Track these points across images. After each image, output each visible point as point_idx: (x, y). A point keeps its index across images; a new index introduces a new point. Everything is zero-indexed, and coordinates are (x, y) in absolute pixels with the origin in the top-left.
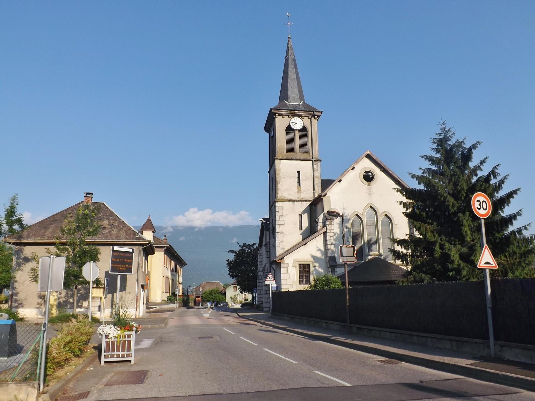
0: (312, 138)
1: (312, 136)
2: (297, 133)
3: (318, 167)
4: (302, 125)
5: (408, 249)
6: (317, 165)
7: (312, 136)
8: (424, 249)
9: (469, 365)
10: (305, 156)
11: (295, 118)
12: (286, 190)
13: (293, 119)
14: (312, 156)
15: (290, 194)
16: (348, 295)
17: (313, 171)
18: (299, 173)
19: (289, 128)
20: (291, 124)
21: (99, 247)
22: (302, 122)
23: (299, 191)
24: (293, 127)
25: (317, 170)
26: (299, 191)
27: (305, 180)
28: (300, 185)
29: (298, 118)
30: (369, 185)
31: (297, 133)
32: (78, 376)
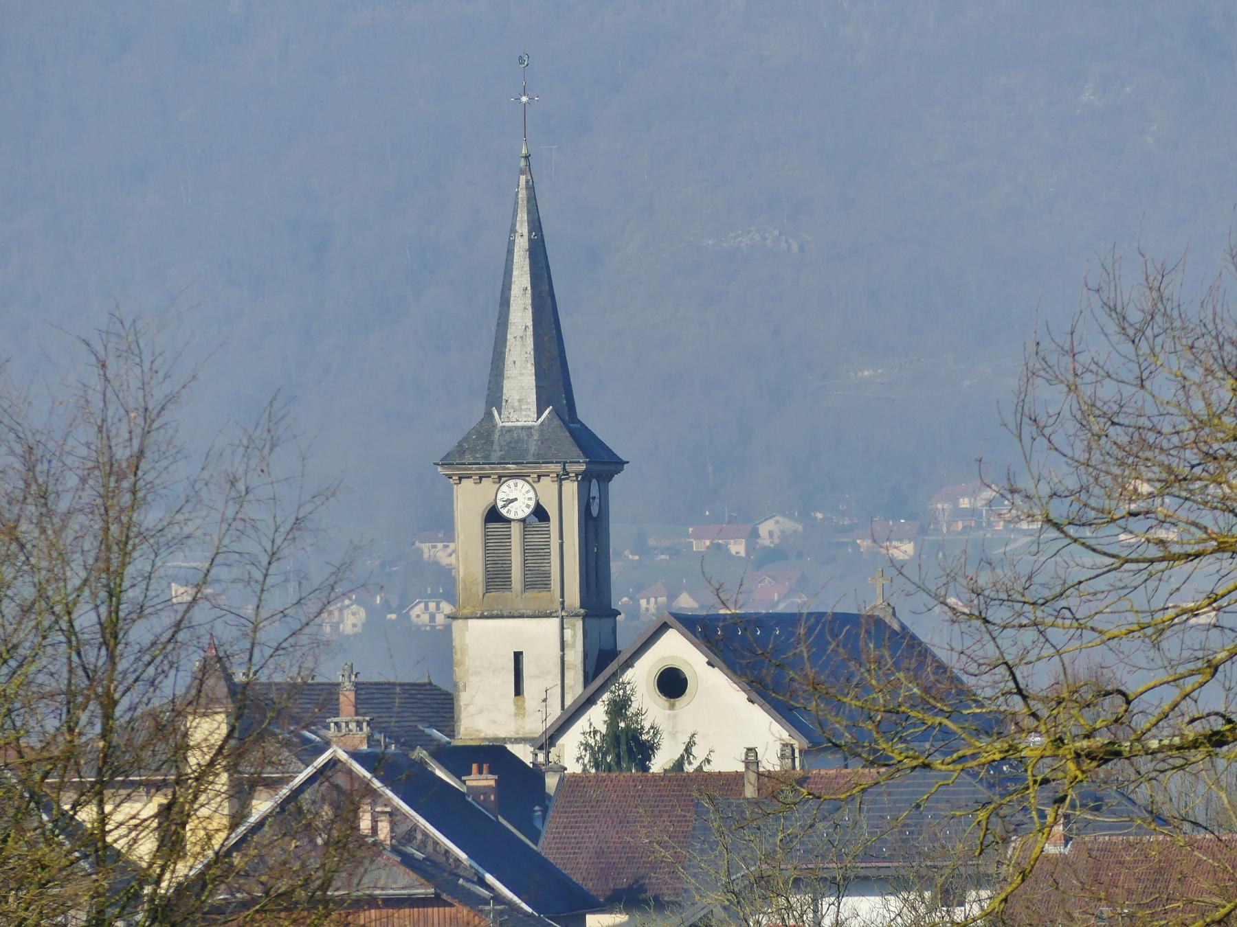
0: (561, 546)
1: (561, 537)
2: (516, 529)
3: (574, 636)
4: (532, 504)
5: (422, 764)
6: (573, 627)
7: (561, 537)
8: (535, 776)
9: (403, 888)
10: (537, 598)
11: (511, 482)
12: (481, 712)
13: (504, 488)
14: (563, 603)
15: (494, 722)
16: (530, 910)
17: (563, 649)
18: (518, 656)
19: (493, 515)
20: (500, 504)
21: (1162, 554)
22: (532, 494)
23: (520, 711)
24: (504, 512)
25: (573, 645)
26: (520, 711)
27: (537, 677)
28: (518, 691)
29: (520, 483)
30: (672, 707)
31: (516, 529)
32: (1025, 848)
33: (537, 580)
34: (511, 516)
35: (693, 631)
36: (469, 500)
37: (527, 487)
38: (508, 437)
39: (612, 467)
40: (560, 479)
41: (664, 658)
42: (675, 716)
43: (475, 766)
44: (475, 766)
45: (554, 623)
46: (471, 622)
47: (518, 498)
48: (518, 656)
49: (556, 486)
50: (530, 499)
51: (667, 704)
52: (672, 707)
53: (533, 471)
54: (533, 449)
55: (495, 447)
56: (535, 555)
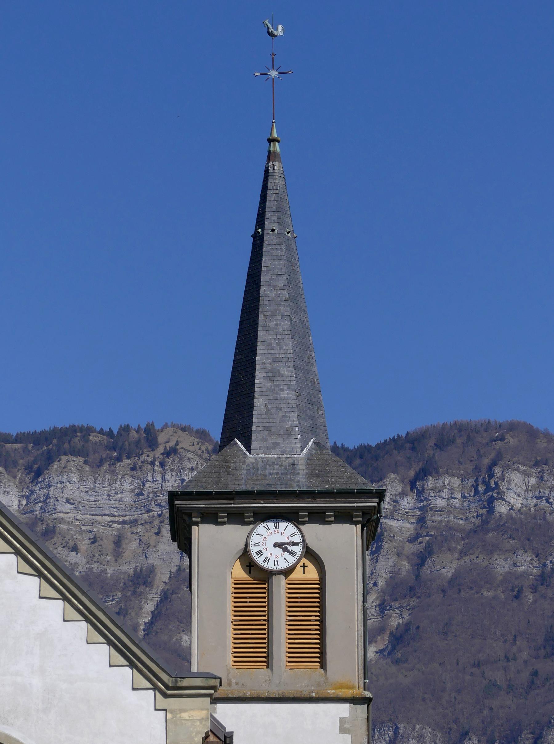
47: (272, 542)
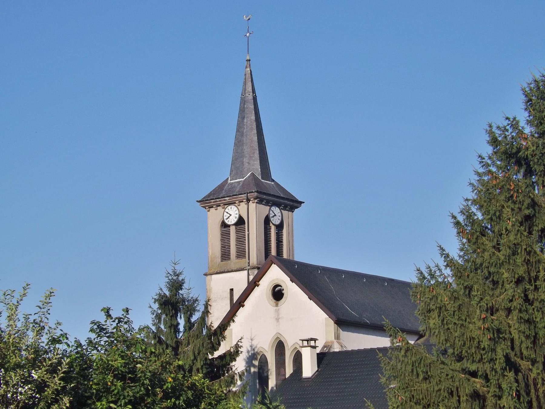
1: (248, 231)
4: (237, 216)
7: (248, 231)
10: (243, 262)
11: (229, 207)
14: (249, 263)
18: (232, 290)
19: (224, 225)
22: (237, 212)
29: (233, 207)
30: (277, 305)
33: (241, 253)
34: (229, 223)
35: (286, 267)
36: (214, 216)
37: (236, 208)
38: (230, 187)
39: (295, 204)
40: (248, 200)
41: (273, 280)
42: (279, 310)
43: (309, 369)
44: (309, 369)
45: (246, 272)
46: (213, 276)
47: (232, 214)
48: (232, 290)
49: (246, 206)
50: (236, 214)
51: (275, 304)
52: (277, 305)
53: (236, 199)
54: (237, 189)
55: (224, 191)
56: (241, 241)
